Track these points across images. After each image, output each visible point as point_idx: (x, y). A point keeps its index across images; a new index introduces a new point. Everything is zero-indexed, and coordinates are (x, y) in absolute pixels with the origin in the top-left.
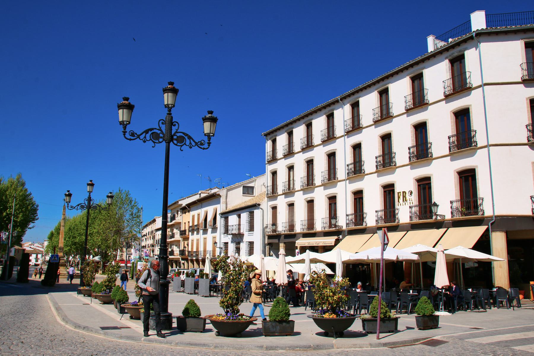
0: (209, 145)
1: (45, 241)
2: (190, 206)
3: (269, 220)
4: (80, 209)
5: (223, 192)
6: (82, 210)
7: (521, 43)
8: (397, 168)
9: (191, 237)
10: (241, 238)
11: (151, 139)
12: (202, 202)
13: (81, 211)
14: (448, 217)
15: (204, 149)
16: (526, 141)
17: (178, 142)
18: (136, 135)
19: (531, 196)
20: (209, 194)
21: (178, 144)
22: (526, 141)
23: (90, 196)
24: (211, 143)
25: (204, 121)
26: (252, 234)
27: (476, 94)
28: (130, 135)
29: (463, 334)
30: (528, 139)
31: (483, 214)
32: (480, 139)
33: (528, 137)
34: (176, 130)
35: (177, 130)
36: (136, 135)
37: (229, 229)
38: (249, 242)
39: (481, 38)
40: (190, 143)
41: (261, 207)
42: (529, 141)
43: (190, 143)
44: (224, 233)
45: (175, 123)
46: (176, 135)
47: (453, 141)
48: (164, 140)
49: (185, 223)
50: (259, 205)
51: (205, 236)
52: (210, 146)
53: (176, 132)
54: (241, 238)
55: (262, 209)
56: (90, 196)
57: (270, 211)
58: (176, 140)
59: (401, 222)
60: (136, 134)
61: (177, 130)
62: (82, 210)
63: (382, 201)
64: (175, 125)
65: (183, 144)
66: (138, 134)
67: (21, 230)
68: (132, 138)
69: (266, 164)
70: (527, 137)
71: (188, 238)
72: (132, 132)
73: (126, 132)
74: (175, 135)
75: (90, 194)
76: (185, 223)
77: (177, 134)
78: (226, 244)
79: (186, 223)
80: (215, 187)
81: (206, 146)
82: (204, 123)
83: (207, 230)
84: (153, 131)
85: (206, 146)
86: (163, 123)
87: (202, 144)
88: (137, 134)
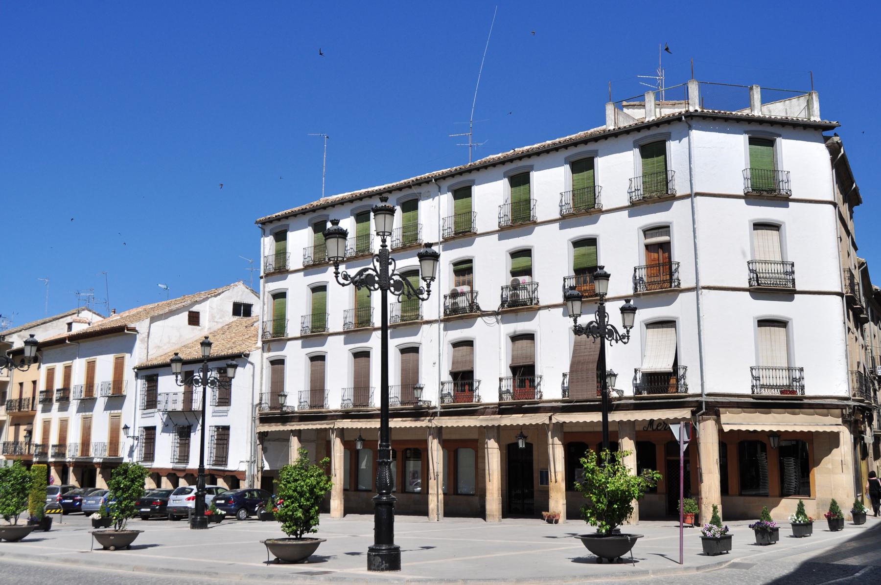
0: (429, 295)
2: (41, 347)
3: (265, 386)
5: (142, 326)
7: (787, 259)
8: (540, 309)
9: (40, 418)
10: (196, 418)
12: (79, 341)
14: (435, 402)
16: (747, 286)
18: (349, 279)
19: (751, 367)
20: (89, 324)
21: (396, 293)
22: (747, 286)
24: (431, 291)
25: (327, 237)
26: (152, 415)
27: (679, 209)
28: (343, 279)
30: (749, 282)
31: (541, 396)
32: (685, 277)
33: (750, 279)
36: (349, 279)
37: (194, 398)
38: (216, 426)
39: (693, 123)
41: (250, 359)
42: (750, 286)
43: (409, 292)
44: (217, 404)
46: (393, 279)
47: (641, 276)
49: (21, 384)
50: (247, 356)
51: (63, 415)
52: (430, 295)
54: (196, 418)
55: (252, 364)
57: (267, 369)
58: (393, 286)
59: (545, 398)
60: (349, 276)
65: (401, 292)
68: (346, 282)
69: (261, 278)
70: (749, 279)
71: (32, 417)
72: (345, 273)
73: (339, 273)
76: (21, 384)
77: (393, 277)
78: (150, 431)
79: (24, 385)
80: (83, 308)
82: (326, 240)
83: (95, 400)
88: (351, 277)
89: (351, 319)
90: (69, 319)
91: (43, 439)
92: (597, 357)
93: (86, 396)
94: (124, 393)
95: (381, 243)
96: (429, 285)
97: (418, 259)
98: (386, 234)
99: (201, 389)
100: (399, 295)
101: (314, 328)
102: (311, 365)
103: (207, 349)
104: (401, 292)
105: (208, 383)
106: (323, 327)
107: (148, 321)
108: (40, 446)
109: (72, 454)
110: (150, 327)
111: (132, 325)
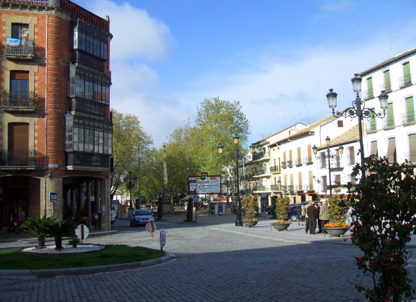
0: (385, 115)
1: (222, 153)
4: (349, 116)
6: (352, 117)
11: (349, 116)
13: (351, 119)
15: (381, 118)
17: (365, 115)
18: (340, 114)
21: (366, 117)
23: (358, 96)
29: (42, 272)
34: (363, 108)
35: (364, 107)
40: (373, 115)
43: (373, 115)
44: (350, 164)
45: (362, 102)
48: (357, 115)
53: (364, 109)
56: (358, 96)
61: (364, 107)
62: (352, 117)
63: (301, 241)
64: (362, 104)
65: (369, 116)
66: (342, 113)
67: (83, 183)
74: (363, 111)
75: (358, 94)
77: (364, 110)
79: (276, 160)
81: (383, 116)
84: (350, 110)
85: (383, 116)
86: (355, 103)
87: (380, 115)
89: (406, 119)
90: (289, 130)
91: (285, 183)
92: (394, 152)
93: (298, 164)
94: (313, 162)
95: (356, 95)
96: (384, 111)
97: (379, 99)
98: (358, 91)
99: (328, 159)
100: (368, 118)
101: (389, 125)
102: (409, 138)
103: (328, 141)
104: (369, 116)
105: (330, 157)
106: (393, 124)
107: (319, 126)
108: (166, 203)
109: (296, 190)
110: (320, 129)
111: (311, 131)
